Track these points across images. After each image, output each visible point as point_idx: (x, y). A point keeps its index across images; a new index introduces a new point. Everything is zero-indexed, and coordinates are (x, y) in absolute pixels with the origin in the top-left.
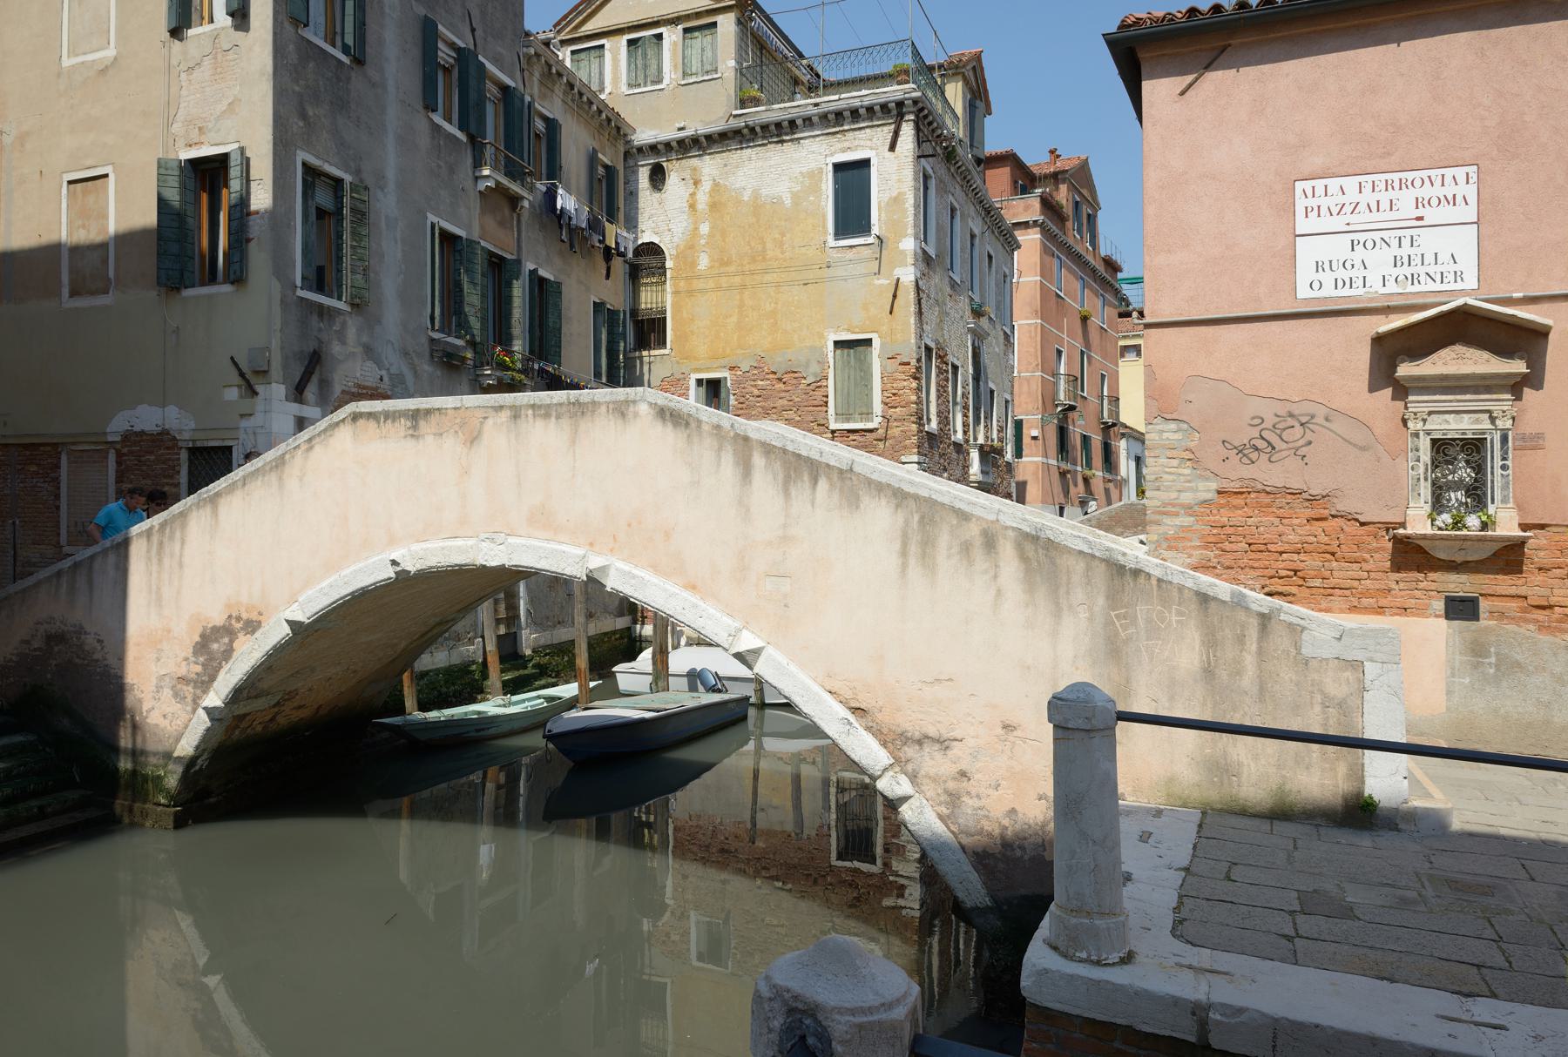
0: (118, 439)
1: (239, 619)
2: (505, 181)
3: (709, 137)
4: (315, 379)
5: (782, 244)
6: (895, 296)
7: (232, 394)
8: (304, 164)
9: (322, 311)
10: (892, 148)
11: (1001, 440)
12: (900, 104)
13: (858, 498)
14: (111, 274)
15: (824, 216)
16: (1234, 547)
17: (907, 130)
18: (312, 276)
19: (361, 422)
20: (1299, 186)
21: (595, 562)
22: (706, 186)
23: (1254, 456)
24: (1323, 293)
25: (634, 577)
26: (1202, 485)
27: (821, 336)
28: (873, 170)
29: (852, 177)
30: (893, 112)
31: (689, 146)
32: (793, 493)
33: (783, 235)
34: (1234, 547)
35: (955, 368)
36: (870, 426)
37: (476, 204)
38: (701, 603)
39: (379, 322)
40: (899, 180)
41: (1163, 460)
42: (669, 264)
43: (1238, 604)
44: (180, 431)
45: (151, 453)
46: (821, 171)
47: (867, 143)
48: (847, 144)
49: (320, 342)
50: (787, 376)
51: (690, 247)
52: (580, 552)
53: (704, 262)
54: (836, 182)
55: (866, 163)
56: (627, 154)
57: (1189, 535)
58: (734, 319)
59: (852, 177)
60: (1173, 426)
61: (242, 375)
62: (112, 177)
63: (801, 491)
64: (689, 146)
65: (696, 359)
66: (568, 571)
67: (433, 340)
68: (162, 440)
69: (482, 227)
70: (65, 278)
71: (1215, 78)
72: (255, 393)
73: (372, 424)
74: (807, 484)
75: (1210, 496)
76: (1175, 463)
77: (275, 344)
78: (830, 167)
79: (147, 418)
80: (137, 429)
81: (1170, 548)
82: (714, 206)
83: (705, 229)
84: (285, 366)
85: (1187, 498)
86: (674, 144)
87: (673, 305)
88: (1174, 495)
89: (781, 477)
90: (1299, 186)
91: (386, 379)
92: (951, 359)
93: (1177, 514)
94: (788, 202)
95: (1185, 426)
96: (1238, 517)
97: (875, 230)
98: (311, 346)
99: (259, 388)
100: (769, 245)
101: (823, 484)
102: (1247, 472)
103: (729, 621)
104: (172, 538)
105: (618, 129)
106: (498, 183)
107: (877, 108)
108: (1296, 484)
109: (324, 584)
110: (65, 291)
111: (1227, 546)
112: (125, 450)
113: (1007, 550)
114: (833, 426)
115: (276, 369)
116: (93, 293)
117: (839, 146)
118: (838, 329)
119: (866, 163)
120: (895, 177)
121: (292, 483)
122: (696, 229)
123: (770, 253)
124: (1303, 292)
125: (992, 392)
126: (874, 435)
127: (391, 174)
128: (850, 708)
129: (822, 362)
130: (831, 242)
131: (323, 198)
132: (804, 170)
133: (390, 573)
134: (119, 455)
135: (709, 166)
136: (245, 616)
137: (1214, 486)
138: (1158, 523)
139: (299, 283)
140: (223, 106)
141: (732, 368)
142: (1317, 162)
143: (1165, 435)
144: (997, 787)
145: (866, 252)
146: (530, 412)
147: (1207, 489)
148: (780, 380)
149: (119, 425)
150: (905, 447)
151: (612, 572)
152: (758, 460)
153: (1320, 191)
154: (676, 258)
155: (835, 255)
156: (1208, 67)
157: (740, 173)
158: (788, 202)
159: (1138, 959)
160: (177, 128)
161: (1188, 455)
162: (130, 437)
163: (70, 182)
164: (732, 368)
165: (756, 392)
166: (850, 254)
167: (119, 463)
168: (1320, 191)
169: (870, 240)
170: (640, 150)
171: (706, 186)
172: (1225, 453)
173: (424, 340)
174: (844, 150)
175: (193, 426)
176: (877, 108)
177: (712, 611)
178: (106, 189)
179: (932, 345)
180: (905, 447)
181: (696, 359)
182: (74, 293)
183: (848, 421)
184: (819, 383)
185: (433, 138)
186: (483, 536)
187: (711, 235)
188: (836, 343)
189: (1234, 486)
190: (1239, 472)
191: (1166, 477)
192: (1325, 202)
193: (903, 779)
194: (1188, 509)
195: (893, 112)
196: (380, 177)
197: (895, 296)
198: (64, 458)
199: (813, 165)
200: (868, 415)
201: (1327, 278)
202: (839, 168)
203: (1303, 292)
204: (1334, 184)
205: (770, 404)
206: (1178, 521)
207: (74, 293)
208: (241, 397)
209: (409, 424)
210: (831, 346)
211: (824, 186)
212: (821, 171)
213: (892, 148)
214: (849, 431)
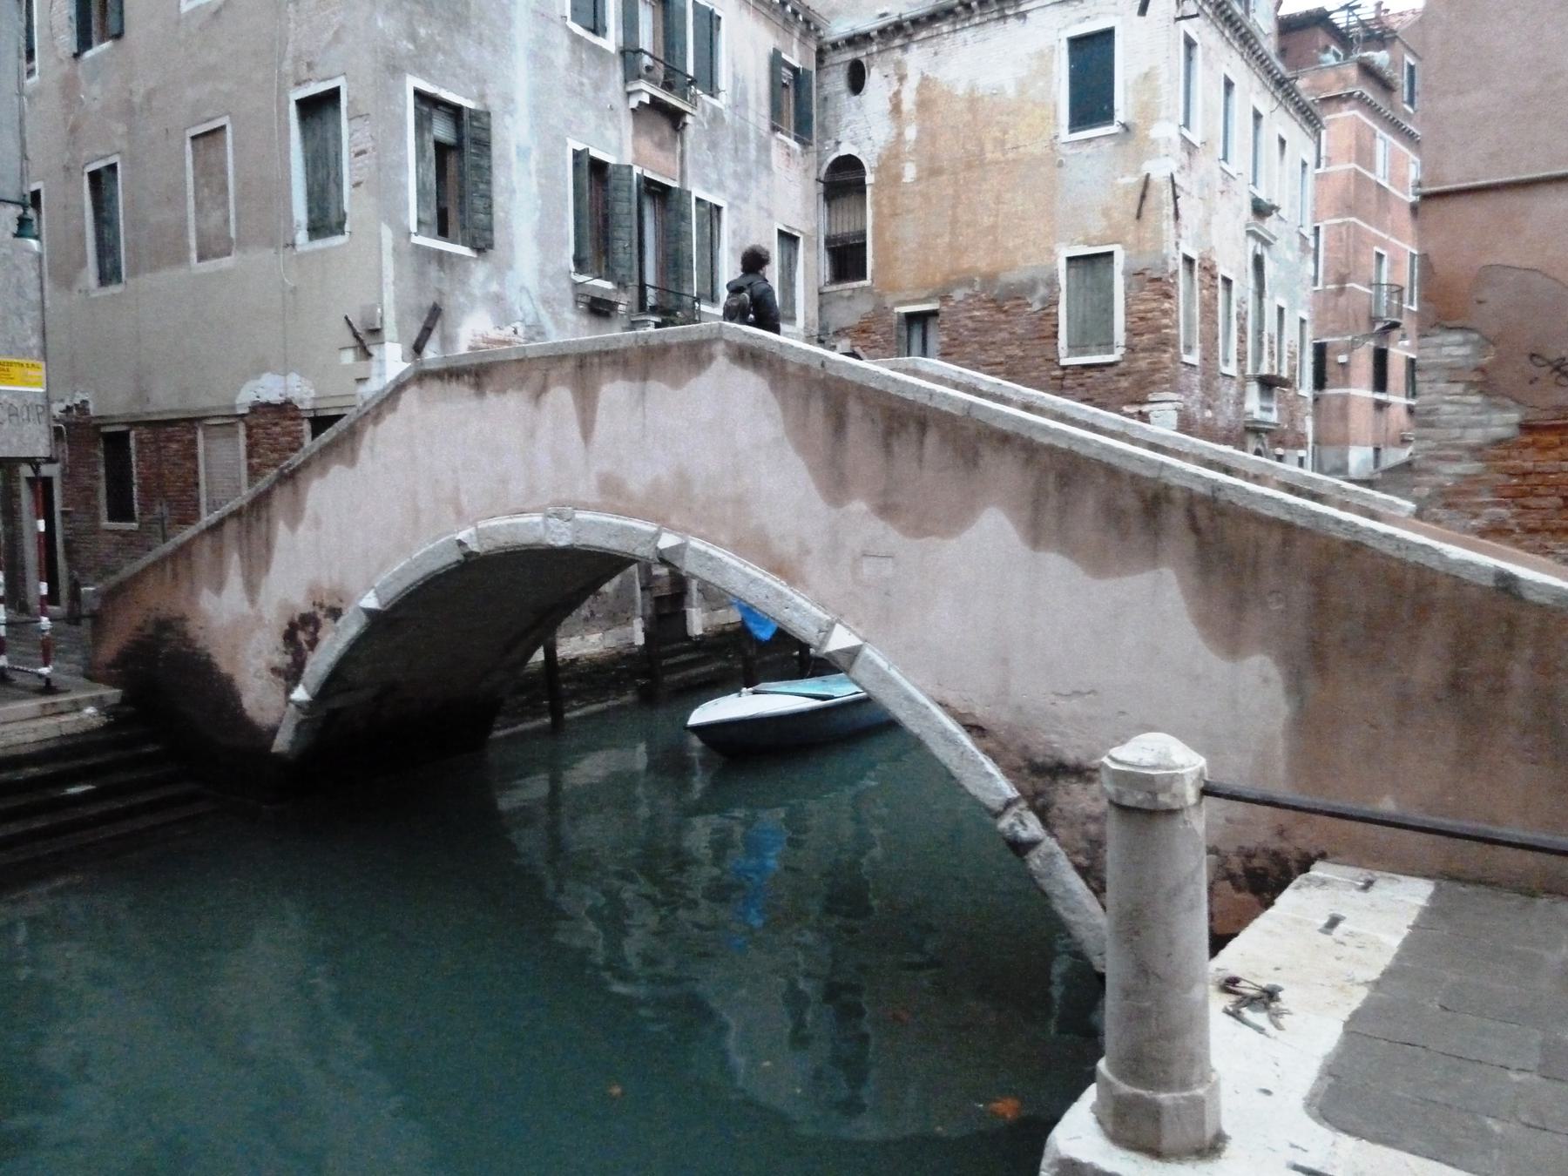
0: (246, 411)
1: (321, 606)
2: (661, 95)
3: (915, 22)
4: (435, 336)
5: (1003, 143)
6: (1143, 197)
7: (348, 357)
8: (419, 94)
9: (441, 257)
11: (1292, 369)
13: (977, 453)
14: (233, 235)
16: (1543, 503)
18: (431, 215)
22: (913, 81)
25: (711, 558)
27: (1051, 252)
31: (899, 31)
32: (896, 449)
33: (1005, 132)
34: (1543, 503)
35: (1228, 282)
37: (627, 124)
38: (786, 590)
39: (510, 267)
41: (1441, 386)
42: (870, 179)
43: (1506, 590)
44: (301, 402)
45: (276, 424)
46: (1052, 49)
48: (1084, 13)
49: (440, 293)
50: (1005, 299)
51: (892, 157)
53: (910, 172)
54: (1072, 60)
55: (1108, 34)
56: (821, 54)
57: (1477, 487)
58: (947, 239)
61: (356, 335)
62: (229, 129)
63: (904, 448)
65: (900, 289)
67: (576, 285)
68: (285, 409)
69: (636, 150)
70: (193, 243)
72: (369, 355)
74: (914, 437)
76: (1459, 388)
77: (389, 297)
78: (1065, 45)
79: (269, 388)
80: (263, 399)
81: (1448, 506)
82: (924, 105)
83: (911, 133)
84: (400, 323)
86: (874, 34)
87: (875, 227)
88: (1457, 432)
89: (880, 427)
91: (520, 331)
92: (1222, 271)
93: (1458, 460)
94: (1011, 92)
95: (1475, 336)
96: (1549, 462)
97: (1120, 116)
98: (428, 302)
99: (373, 350)
100: (989, 147)
101: (932, 439)
104: (259, 519)
105: (807, 22)
106: (653, 98)
110: (194, 255)
112: (253, 423)
114: (1064, 362)
115: (390, 330)
116: (217, 256)
118: (1072, 242)
119: (1108, 34)
121: (364, 454)
122: (900, 134)
123: (989, 156)
125: (1281, 310)
126: (1115, 370)
127: (522, 97)
128: (965, 726)
129: (1052, 283)
130: (1065, 135)
131: (442, 130)
133: (455, 556)
134: (249, 428)
136: (327, 603)
137: (1514, 417)
138: (1428, 471)
139: (413, 227)
140: (328, 36)
143: (1446, 350)
146: (596, 360)
147: (1503, 422)
149: (245, 398)
152: (854, 409)
154: (877, 171)
155: (1068, 150)
158: (1011, 92)
159: (1231, 1149)
160: (287, 66)
161: (1476, 377)
162: (259, 408)
163: (194, 138)
165: (971, 324)
166: (1088, 149)
167: (249, 436)
170: (835, 46)
171: (913, 81)
172: (1533, 371)
173: (566, 285)
174: (1082, 20)
175: (313, 393)
178: (224, 142)
179: (1194, 255)
181: (900, 289)
182: (201, 258)
183: (1083, 353)
184: (1048, 314)
185: (573, 52)
186: (551, 510)
187: (918, 141)
188: (1070, 259)
191: (1447, 408)
194: (1476, 451)
196: (508, 99)
198: (200, 434)
200: (1108, 346)
202: (1076, 43)
206: (1458, 468)
207: (201, 258)
208: (357, 359)
209: (472, 380)
210: (1062, 265)
211: (1055, 68)
212: (1052, 49)
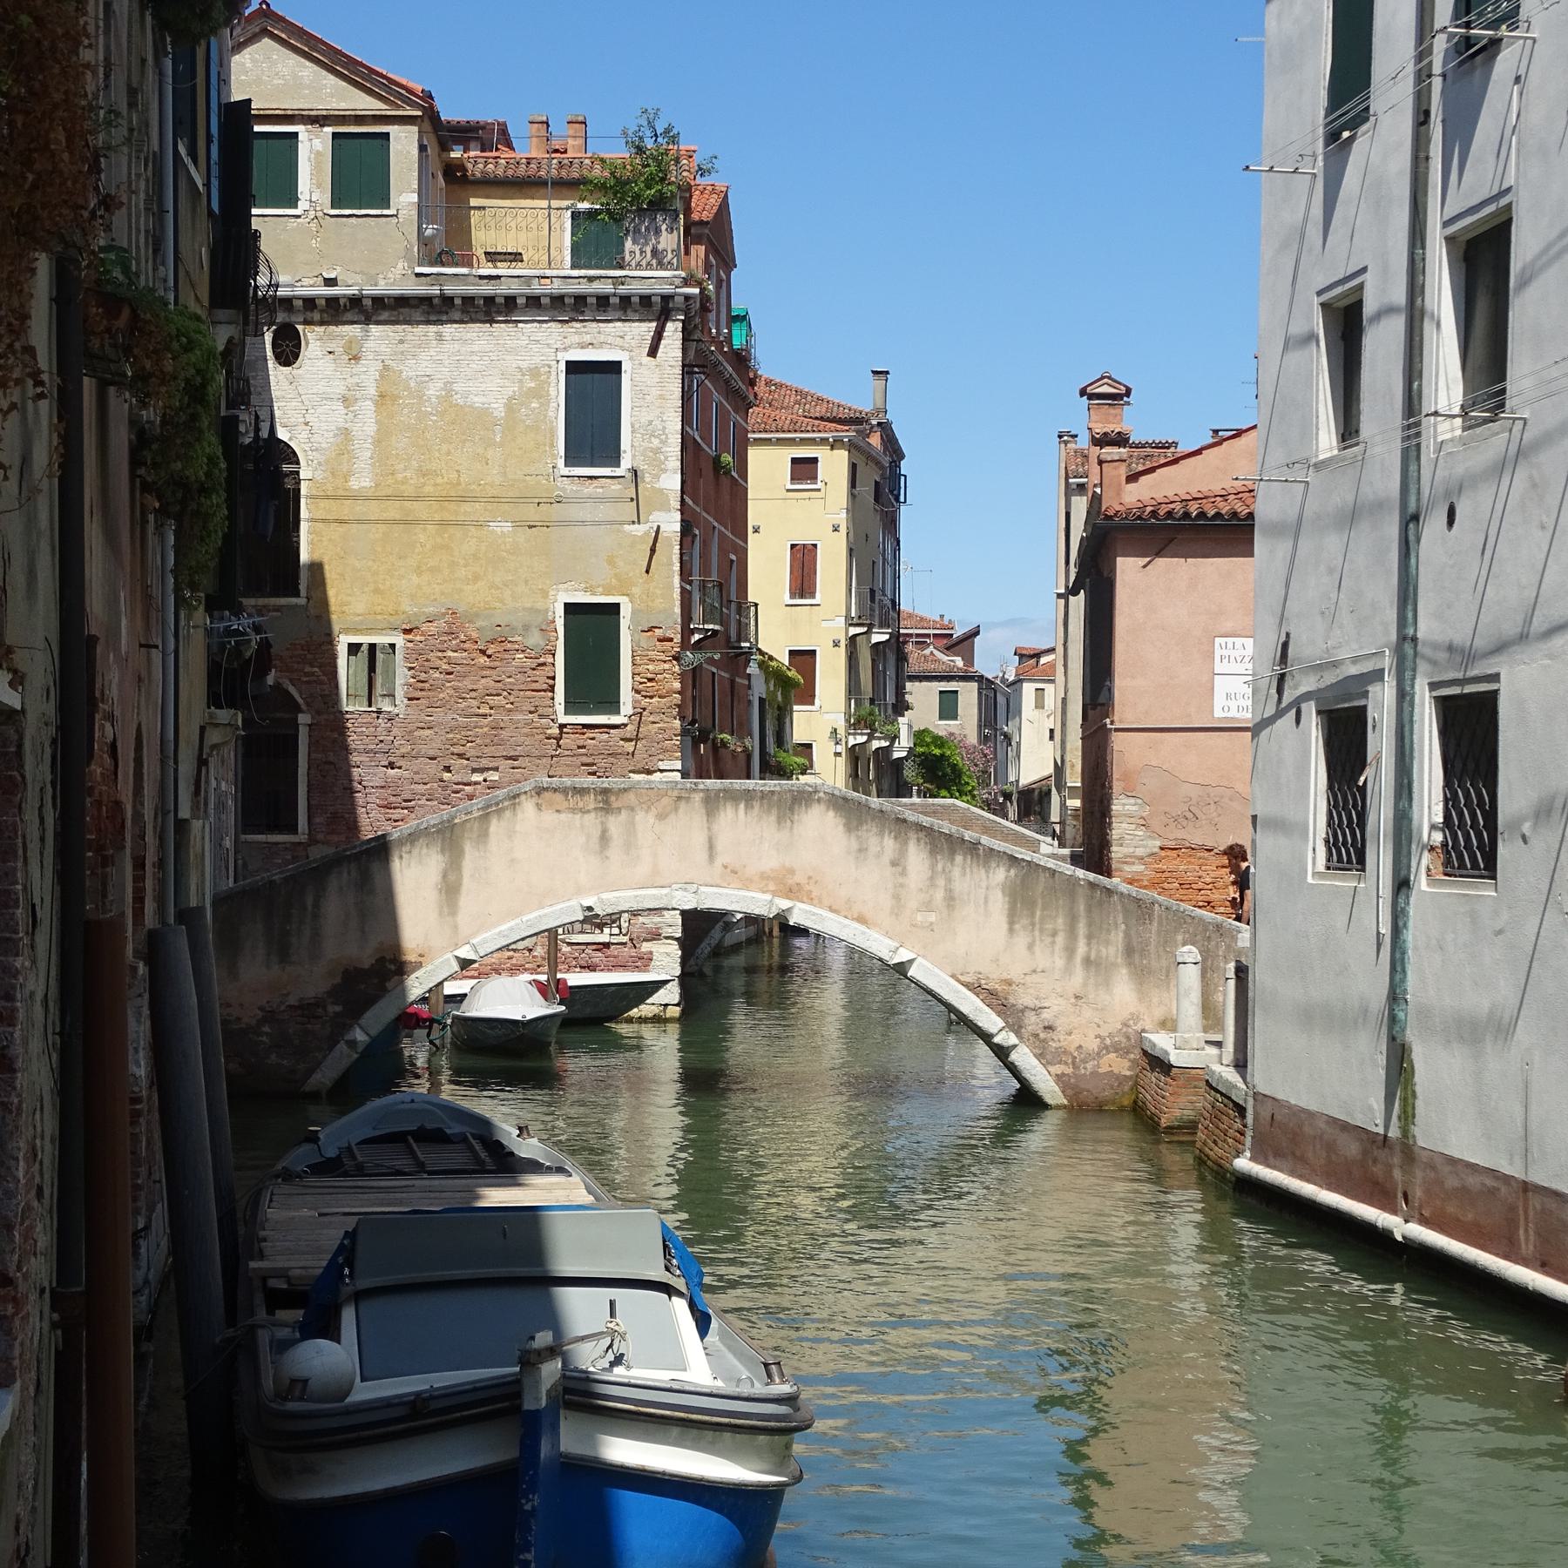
6: (653, 550)
10: (653, 352)
12: (666, 298)
15: (553, 432)
17: (673, 330)
19: (546, 795)
20: (1218, 640)
21: (784, 904)
23: (1185, 823)
24: (1229, 715)
26: (1150, 843)
28: (625, 378)
29: (593, 386)
30: (658, 309)
31: (336, 310)
36: (615, 720)
40: (661, 397)
47: (617, 341)
48: (587, 339)
52: (768, 897)
59: (593, 386)
60: (1132, 801)
64: (336, 310)
66: (757, 912)
71: (1161, 562)
73: (559, 797)
75: (1157, 850)
78: (563, 366)
85: (1140, 852)
90: (1218, 640)
97: (626, 462)
102: (1180, 834)
103: (890, 942)
107: (635, 300)
108: (1210, 844)
109: (504, 927)
111: (1166, 885)
113: (1081, 894)
117: (576, 339)
119: (614, 368)
120: (655, 392)
124: (1218, 713)
132: (524, 365)
135: (380, 338)
137: (1158, 843)
141: (407, 632)
142: (1228, 625)
144: (1070, 1034)
145: (615, 486)
148: (483, 652)
150: (665, 751)
151: (795, 911)
153: (1230, 645)
155: (561, 483)
156: (1158, 554)
157: (423, 356)
164: (407, 632)
166: (590, 489)
168: (1230, 645)
169: (618, 472)
174: (583, 346)
176: (635, 300)
177: (877, 936)
180: (665, 751)
189: (1172, 844)
190: (1175, 835)
192: (1233, 653)
193: (1012, 1035)
195: (658, 309)
197: (653, 550)
199: (537, 360)
201: (1233, 704)
202: (573, 368)
203: (1218, 713)
204: (1239, 641)
205: (467, 684)
210: (560, 611)
213: (653, 352)
214: (585, 726)
